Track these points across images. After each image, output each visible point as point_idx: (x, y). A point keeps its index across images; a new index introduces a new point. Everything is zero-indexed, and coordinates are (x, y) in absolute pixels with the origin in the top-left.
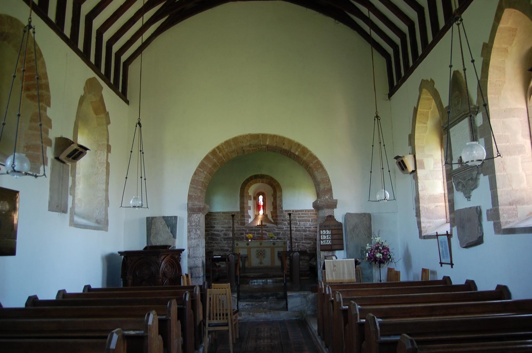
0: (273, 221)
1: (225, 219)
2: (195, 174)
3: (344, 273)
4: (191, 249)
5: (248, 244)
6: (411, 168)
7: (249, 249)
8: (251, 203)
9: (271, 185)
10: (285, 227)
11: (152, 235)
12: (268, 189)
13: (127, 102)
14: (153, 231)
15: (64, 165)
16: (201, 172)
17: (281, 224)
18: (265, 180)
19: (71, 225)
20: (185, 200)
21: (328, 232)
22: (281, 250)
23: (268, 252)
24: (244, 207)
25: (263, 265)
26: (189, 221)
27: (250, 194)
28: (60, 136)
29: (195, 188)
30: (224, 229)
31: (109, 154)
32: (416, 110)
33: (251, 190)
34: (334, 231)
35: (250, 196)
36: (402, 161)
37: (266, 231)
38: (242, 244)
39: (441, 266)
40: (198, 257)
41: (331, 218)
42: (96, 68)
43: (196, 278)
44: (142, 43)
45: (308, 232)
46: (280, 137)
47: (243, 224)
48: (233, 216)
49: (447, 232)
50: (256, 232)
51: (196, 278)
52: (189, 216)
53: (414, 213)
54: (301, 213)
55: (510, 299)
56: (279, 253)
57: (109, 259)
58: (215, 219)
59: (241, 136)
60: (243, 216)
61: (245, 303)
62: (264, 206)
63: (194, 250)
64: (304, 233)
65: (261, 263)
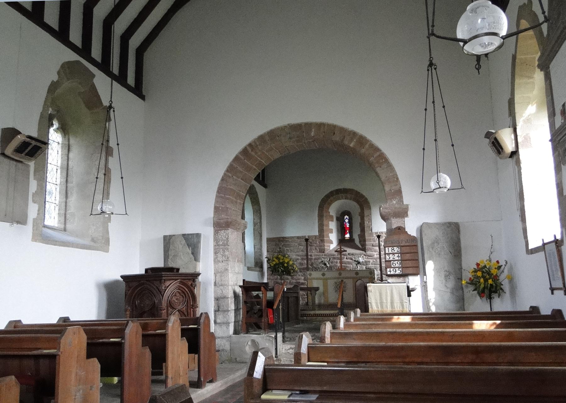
0: (360, 246)
1: (300, 245)
3: (392, 303)
4: (218, 275)
5: (323, 275)
6: (509, 147)
7: (325, 280)
8: (333, 225)
9: (358, 202)
10: (375, 253)
11: (170, 257)
12: (352, 206)
13: (143, 97)
14: (171, 253)
15: (20, 165)
16: (229, 177)
18: (349, 196)
19: (34, 239)
20: (210, 213)
21: (396, 249)
24: (323, 230)
26: (216, 240)
27: (331, 214)
28: (11, 127)
29: (221, 197)
30: (300, 258)
31: (110, 158)
32: (514, 58)
33: (333, 210)
34: (404, 248)
35: (332, 217)
36: (496, 139)
38: (315, 274)
39: (552, 293)
40: (226, 285)
41: (401, 230)
42: (85, 50)
43: (225, 311)
44: (115, 6)
46: (329, 125)
47: (322, 251)
48: (307, 240)
49: (555, 236)
51: (225, 311)
52: (216, 232)
53: (518, 213)
55: (464, 310)
57: (110, 288)
58: (289, 246)
59: (278, 128)
60: (322, 241)
61: (289, 346)
63: (221, 276)
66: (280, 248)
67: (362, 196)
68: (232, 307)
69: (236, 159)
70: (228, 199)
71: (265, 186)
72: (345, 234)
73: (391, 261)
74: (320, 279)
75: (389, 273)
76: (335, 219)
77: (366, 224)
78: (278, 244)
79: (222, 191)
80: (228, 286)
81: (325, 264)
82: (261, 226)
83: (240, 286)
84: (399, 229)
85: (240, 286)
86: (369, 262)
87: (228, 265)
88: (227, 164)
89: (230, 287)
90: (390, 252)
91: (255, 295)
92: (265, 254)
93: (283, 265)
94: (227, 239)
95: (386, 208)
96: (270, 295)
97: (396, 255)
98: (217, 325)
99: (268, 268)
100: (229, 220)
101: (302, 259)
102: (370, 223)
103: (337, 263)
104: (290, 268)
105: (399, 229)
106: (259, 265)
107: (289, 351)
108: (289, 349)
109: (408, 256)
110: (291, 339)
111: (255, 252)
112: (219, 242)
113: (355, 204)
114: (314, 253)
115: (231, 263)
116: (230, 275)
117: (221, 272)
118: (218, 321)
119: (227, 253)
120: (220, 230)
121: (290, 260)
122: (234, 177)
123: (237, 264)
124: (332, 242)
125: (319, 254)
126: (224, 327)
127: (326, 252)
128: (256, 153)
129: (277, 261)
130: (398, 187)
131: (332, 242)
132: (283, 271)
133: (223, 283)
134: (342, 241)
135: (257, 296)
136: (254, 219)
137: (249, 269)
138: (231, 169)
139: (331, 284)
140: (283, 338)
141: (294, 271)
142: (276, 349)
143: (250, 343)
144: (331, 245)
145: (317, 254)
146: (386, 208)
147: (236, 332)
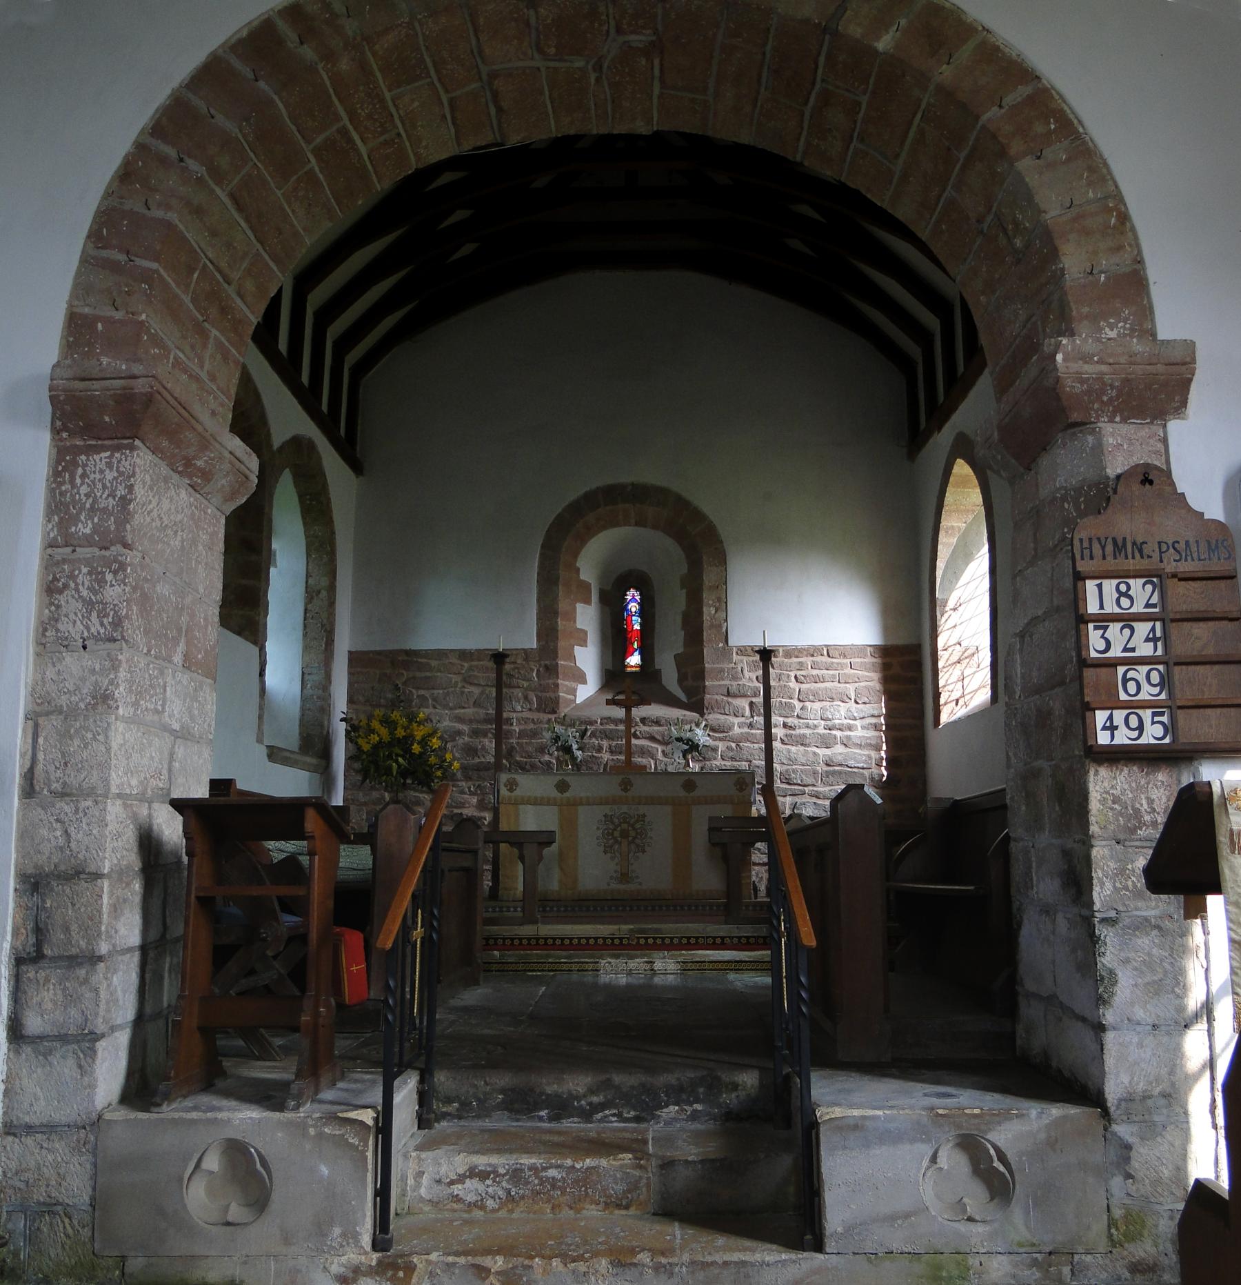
0: (683, 697)
1: (468, 681)
2: (127, 174)
4: (50, 725)
5: (562, 786)
7: (568, 808)
8: (587, 617)
9: (680, 536)
10: (736, 721)
12: (661, 551)
16: (163, 161)
17: (720, 708)
22: (724, 811)
23: (661, 824)
25: (632, 887)
26: (60, 508)
27: (582, 577)
29: (114, 267)
30: (465, 728)
33: (589, 564)
35: (586, 587)
37: (652, 738)
38: (529, 785)
40: (91, 793)
43: (73, 961)
45: (839, 749)
47: (550, 705)
50: (605, 744)
51: (73, 961)
52: (64, 463)
54: (808, 661)
56: (714, 829)
60: (551, 670)
61: (461, 1162)
62: (647, 635)
63: (65, 735)
64: (822, 752)
65: (624, 877)
66: (397, 688)
67: (697, 516)
68: (127, 929)
69: (211, 74)
70: (147, 277)
71: (356, 466)
72: (627, 653)
73: (1113, 664)
74: (549, 802)
75: (1103, 738)
76: (595, 597)
77: (706, 617)
78: (389, 675)
79: (120, 235)
80: (98, 795)
81: (567, 750)
82: (332, 604)
83: (180, 805)
84: (1147, 481)
85: (180, 805)
86: (715, 750)
87: (115, 668)
88: (161, 96)
89: (114, 810)
90: (1111, 608)
91: (277, 857)
92: (340, 703)
93: (407, 752)
94: (125, 502)
95: (1087, 358)
96: (355, 859)
97: (1143, 629)
98: (27, 1049)
99: (350, 759)
100: (141, 386)
101: (475, 733)
102: (722, 615)
103: (600, 749)
104: (433, 760)
105: (1147, 481)
106: (314, 746)
107: (457, 1189)
108: (461, 1179)
109: (1199, 638)
110: (465, 1105)
111: (304, 699)
112: (75, 520)
113: (670, 544)
114: (519, 713)
115: (133, 662)
116: (120, 735)
117: (69, 714)
118: (34, 1024)
119: (112, 593)
120: (90, 450)
121: (432, 735)
122: (192, 164)
123: (177, 682)
124: (582, 679)
125: (535, 716)
126: (65, 1065)
127: (564, 711)
128: (329, 56)
129: (384, 732)
130: (1127, 256)
131: (582, 679)
132: (404, 773)
133: (73, 780)
134: (613, 676)
135: (291, 869)
136: (308, 575)
137: (274, 754)
138: (176, 122)
139: (589, 823)
140: (421, 1103)
141: (444, 777)
142: (383, 1193)
143: (213, 1163)
144: (580, 688)
145: (526, 714)
146: (1087, 358)
147: (140, 1090)
